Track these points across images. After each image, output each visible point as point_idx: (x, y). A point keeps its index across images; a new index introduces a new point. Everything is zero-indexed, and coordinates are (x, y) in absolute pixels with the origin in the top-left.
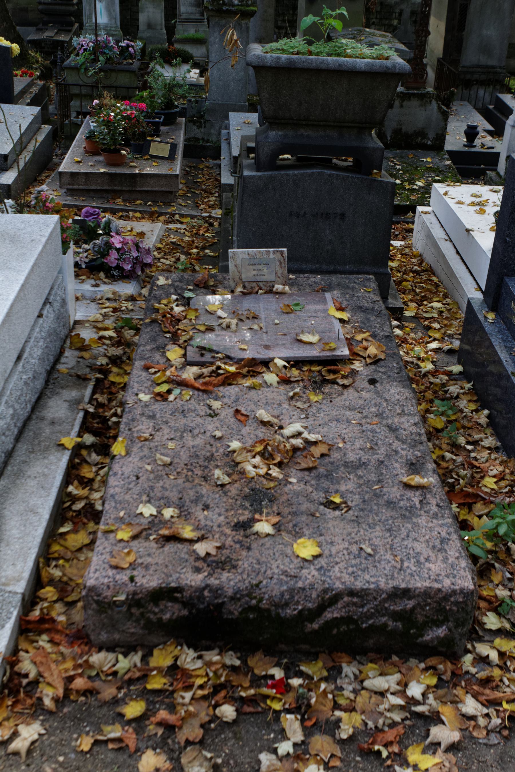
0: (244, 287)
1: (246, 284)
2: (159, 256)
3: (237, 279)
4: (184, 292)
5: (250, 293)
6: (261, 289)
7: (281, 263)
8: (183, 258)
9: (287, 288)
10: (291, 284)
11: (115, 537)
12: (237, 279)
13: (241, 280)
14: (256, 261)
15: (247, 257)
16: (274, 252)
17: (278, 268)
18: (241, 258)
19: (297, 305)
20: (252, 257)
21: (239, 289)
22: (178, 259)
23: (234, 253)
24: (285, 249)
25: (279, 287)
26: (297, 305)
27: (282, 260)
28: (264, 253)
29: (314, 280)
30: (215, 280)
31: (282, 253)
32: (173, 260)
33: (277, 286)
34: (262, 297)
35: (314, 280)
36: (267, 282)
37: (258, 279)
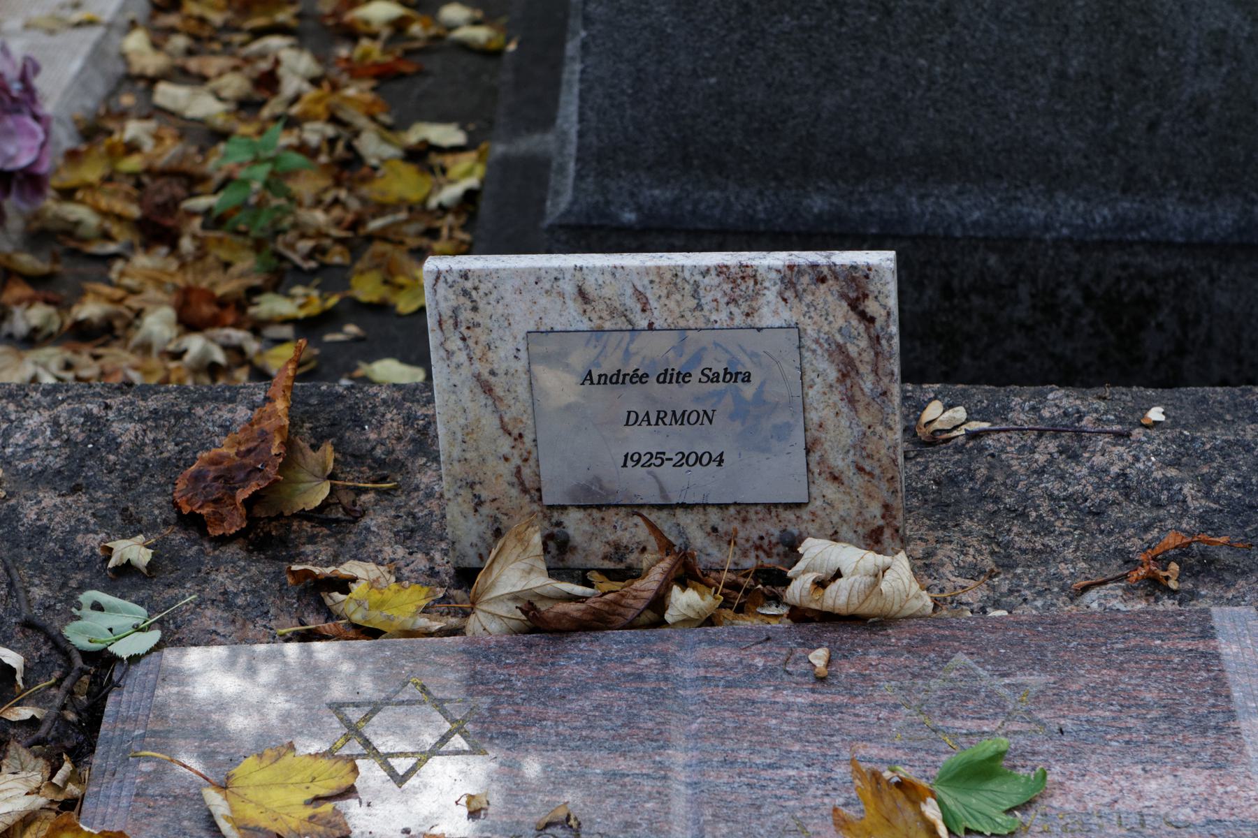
0: (558, 552)
1: (575, 524)
2: (151, 62)
3: (498, 481)
4: (69, 606)
5: (597, 622)
6: (686, 574)
7: (848, 370)
8: (296, 65)
9: (899, 579)
10: (931, 501)
11: (358, 756)
12: (498, 481)
13: (535, 493)
14: (653, 350)
15: (570, 316)
16: (789, 278)
17: (824, 404)
18: (524, 324)
19: (980, 772)
20: (615, 319)
21: (517, 575)
22: (269, 81)
23: (465, 284)
24: (882, 260)
25: (840, 565)
26: (980, 772)
27: (858, 347)
28: (714, 290)
29: (1112, 457)
30: (351, 457)
31: (855, 288)
32: (235, 84)
33: (818, 552)
34: (692, 658)
35: (1112, 457)
36: (743, 508)
37: (680, 482)
